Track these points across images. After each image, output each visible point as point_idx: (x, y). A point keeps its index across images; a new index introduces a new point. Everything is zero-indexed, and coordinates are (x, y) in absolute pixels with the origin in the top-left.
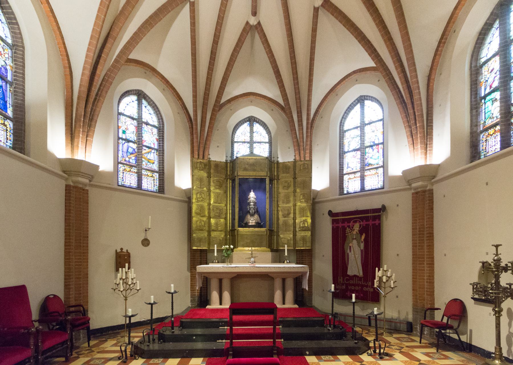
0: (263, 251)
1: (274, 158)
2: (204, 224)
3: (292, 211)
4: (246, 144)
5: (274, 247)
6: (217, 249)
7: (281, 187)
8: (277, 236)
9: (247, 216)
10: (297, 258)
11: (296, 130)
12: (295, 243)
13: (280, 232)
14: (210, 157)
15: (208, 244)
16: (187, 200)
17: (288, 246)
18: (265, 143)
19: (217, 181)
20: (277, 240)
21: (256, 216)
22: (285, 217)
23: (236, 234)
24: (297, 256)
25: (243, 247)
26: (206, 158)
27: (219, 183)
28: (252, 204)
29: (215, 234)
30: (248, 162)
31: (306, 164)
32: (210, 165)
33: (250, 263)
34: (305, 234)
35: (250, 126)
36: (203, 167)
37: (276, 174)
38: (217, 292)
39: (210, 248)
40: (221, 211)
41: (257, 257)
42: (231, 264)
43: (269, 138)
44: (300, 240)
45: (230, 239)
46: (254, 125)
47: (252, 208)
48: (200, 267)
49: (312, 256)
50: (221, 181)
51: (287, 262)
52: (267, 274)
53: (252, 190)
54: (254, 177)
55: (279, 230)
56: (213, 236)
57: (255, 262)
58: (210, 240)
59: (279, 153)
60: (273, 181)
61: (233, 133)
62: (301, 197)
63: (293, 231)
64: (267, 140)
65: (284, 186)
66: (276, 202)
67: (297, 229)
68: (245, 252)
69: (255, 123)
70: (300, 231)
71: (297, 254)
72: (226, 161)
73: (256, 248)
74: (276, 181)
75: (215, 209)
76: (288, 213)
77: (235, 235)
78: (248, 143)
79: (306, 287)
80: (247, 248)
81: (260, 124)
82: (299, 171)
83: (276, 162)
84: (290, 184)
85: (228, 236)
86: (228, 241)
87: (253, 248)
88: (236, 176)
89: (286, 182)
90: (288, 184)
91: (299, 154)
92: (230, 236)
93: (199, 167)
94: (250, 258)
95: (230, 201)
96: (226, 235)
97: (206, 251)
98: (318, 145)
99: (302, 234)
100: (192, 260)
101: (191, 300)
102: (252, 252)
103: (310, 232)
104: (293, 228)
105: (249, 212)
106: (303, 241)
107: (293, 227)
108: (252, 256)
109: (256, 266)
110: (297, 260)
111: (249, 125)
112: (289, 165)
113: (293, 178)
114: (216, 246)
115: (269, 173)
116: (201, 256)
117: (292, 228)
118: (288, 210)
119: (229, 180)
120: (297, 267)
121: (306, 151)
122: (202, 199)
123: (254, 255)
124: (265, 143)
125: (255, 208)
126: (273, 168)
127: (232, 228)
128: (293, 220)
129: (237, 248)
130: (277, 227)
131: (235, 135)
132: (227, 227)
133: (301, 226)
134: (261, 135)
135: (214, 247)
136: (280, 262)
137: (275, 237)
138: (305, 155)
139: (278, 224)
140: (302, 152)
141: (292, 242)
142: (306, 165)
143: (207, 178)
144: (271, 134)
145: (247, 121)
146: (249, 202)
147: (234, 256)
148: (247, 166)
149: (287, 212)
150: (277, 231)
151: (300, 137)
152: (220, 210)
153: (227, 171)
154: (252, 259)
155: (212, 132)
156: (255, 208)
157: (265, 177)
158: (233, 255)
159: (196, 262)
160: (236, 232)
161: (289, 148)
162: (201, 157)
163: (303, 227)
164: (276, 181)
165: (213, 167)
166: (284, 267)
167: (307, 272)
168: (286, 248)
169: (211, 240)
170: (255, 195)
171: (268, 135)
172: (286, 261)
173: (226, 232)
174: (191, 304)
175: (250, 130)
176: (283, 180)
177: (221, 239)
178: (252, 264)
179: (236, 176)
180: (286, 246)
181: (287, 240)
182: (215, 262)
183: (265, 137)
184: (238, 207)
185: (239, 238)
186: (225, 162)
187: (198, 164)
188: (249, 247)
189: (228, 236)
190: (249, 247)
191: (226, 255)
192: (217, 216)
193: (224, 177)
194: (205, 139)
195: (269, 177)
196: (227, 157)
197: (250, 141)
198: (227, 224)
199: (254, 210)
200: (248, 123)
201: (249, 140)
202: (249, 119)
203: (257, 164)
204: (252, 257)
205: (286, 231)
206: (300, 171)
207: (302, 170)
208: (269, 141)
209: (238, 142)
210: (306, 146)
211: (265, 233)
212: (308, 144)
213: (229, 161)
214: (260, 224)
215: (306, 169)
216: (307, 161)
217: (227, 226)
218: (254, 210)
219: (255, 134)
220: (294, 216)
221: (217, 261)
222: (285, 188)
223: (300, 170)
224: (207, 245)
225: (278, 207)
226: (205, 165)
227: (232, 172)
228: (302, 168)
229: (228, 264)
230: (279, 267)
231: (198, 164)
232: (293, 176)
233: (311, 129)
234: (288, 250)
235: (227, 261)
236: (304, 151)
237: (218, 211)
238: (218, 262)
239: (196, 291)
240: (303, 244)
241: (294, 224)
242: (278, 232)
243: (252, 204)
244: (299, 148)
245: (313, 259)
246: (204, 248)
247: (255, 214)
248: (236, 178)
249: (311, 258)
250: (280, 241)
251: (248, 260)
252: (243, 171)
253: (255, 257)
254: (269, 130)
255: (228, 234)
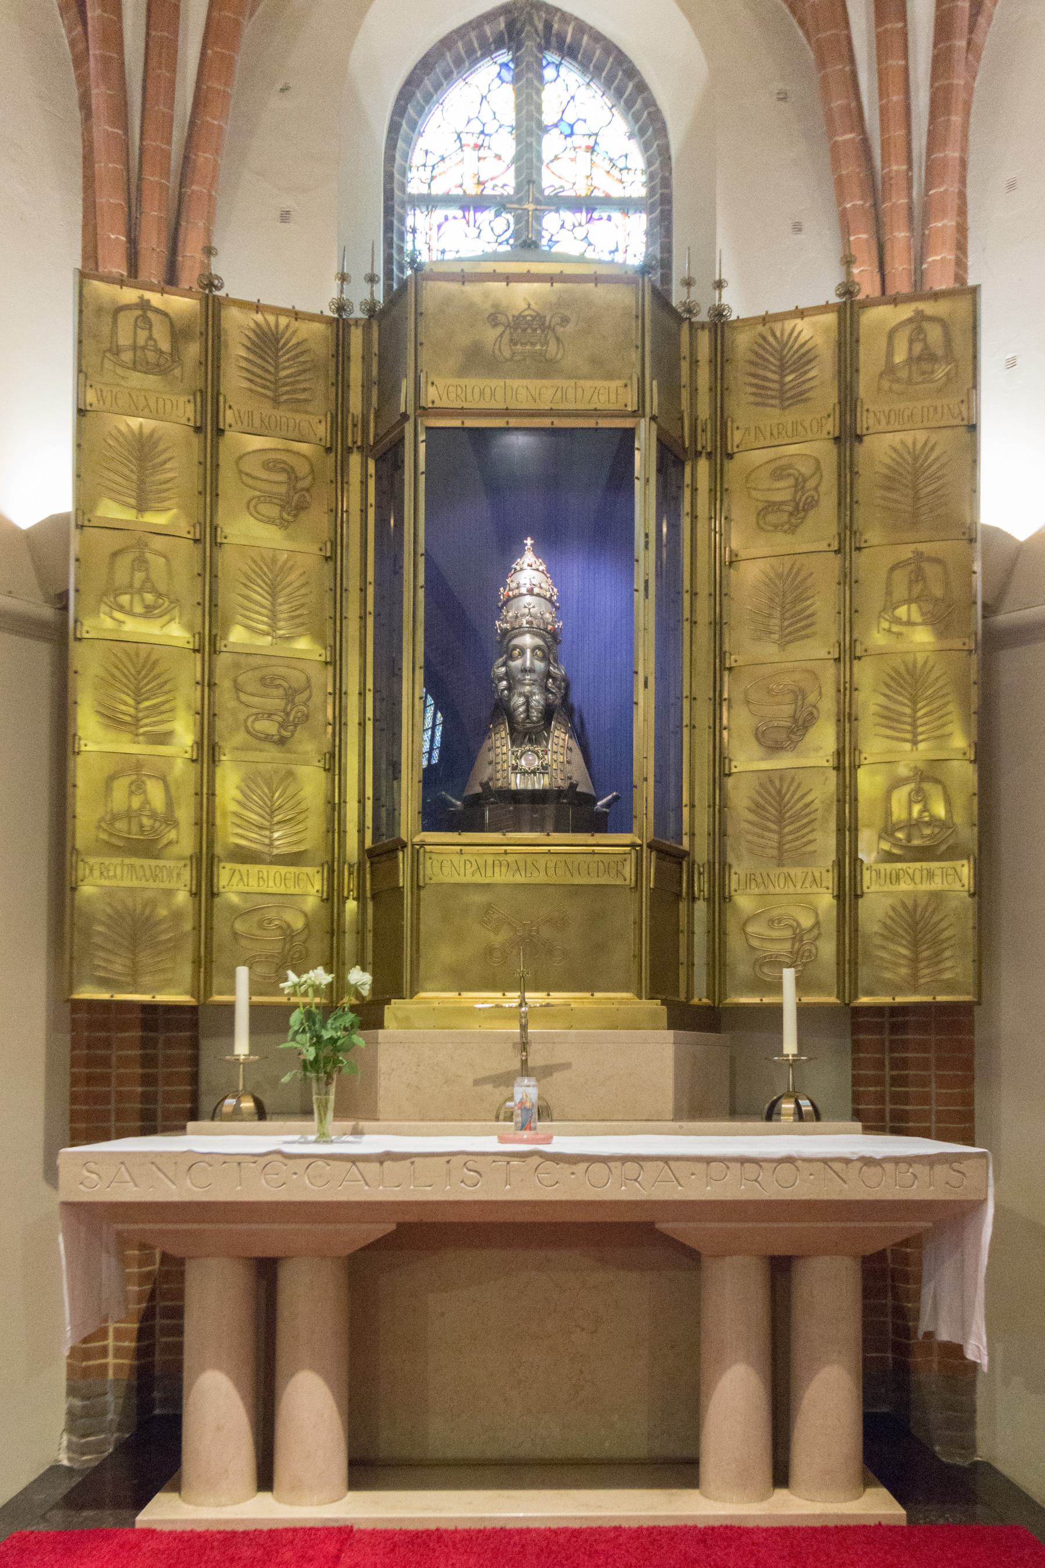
0: (613, 1022)
1: (688, 283)
2: (170, 804)
3: (828, 706)
4: (489, 214)
5: (690, 994)
6: (253, 1008)
7: (740, 509)
8: (710, 900)
9: (488, 743)
10: (856, 1081)
11: (852, 60)
12: (854, 963)
13: (739, 869)
14: (218, 267)
15: (197, 962)
16: (48, 613)
17: (802, 984)
18: (625, 206)
19: (266, 466)
20: (710, 932)
21: (560, 737)
22: (774, 748)
23: (404, 880)
24: (856, 1064)
25: (460, 990)
26: (189, 277)
27: (282, 477)
28: (527, 640)
29: (254, 886)
30: (496, 306)
31: (932, 319)
32: (218, 336)
33: (510, 1117)
34: (926, 887)
35: (516, 79)
36: (165, 346)
37: (704, 411)
38: (237, 1384)
39: (208, 992)
40: (298, 699)
41: (565, 1066)
42: (357, 1132)
43: (649, 163)
44: (889, 934)
45: (364, 922)
46: (549, 73)
47: (524, 671)
48: (86, 1161)
49: (968, 1065)
50: (303, 469)
51: (800, 1115)
52: (644, 1217)
53: (529, 542)
54: (545, 422)
55: (731, 858)
56: (235, 899)
57: (544, 1112)
58: (210, 929)
59: (722, 242)
60: (688, 470)
61: (394, 129)
62: (900, 591)
63: (839, 864)
64: (637, 187)
65: (770, 507)
66: (704, 634)
67: (867, 854)
68: (475, 1028)
69: (551, 57)
70: (889, 857)
71: (857, 1047)
72: (341, 307)
73: (558, 997)
74: (703, 466)
75: (249, 689)
76: (794, 718)
77: (399, 890)
78: (501, 205)
79: (963, 1324)
80: (484, 1000)
81: (584, 67)
82: (881, 375)
83: (703, 317)
84: (811, 484)
85: (351, 905)
86: (349, 942)
87: (535, 998)
88: (405, 417)
89: (779, 473)
90: (800, 484)
91: (874, 253)
92: (360, 898)
93: (134, 347)
94: (506, 1080)
95: (364, 627)
96: (332, 898)
97: (194, 1025)
98: (1011, 186)
99: (905, 886)
100: (81, 1089)
101: (71, 1414)
102: (524, 1028)
103: (965, 870)
104: (832, 841)
105: (502, 710)
106: (915, 945)
107: (833, 826)
108: (524, 1062)
109: (563, 1144)
110: (856, 1098)
111: (507, 76)
112: (805, 336)
113: (837, 439)
114: (242, 974)
115: (653, 387)
116: (148, 1061)
117: (826, 842)
118: (799, 694)
119: (355, 460)
120: (896, 1160)
121: (926, 222)
122: (149, 598)
123: (535, 1060)
124: (625, 206)
125: (548, 675)
126: (685, 365)
127: (374, 840)
128: (833, 775)
129: (412, 995)
130: (711, 834)
131: (409, 142)
132: (342, 832)
133: (898, 812)
134: (591, 149)
135: (232, 991)
136: (735, 1112)
137: (701, 908)
138: (920, 258)
139: (720, 808)
140: (900, 236)
141: (827, 949)
142: (934, 334)
143: (195, 440)
144: (662, 131)
145: (500, 43)
146: (505, 632)
147: (383, 1064)
148: (490, 335)
149: (787, 710)
150: (711, 864)
151: (883, 111)
152: (290, 695)
153: (346, 386)
154: (526, 1091)
155: (228, 63)
156: (548, 675)
157: (627, 423)
158: (381, 1048)
159: (112, 1106)
160: (404, 860)
161: (797, 228)
162: (152, 267)
163: (912, 826)
164: (703, 466)
165: (236, 350)
166: (789, 1160)
167: (976, 1206)
168: (789, 999)
169: (222, 931)
170: (551, 572)
171: (646, 147)
172: (788, 1106)
173: (332, 870)
174: (70, 1447)
175: (518, 108)
176: (758, 457)
177: (298, 924)
178: (523, 1127)
179: (405, 417)
180: (789, 976)
181: (788, 933)
182: (236, 1114)
183: (621, 163)
184: (420, 661)
185: (430, 920)
186: (329, 321)
187: (126, 322)
188: (504, 988)
189: (351, 905)
190: (504, 987)
191: (310, 1054)
192: (267, 738)
193: (322, 430)
194: (178, 135)
195: (653, 418)
196: (343, 278)
197: (518, 188)
198: (343, 802)
199: (547, 690)
200: (504, 56)
201: (512, 183)
202: (510, 25)
203: (565, 320)
204: (525, 1070)
205: (780, 864)
206: (886, 384)
207: (903, 374)
208: (652, 192)
209: (429, 202)
210: (929, 185)
211: (629, 871)
212: (944, 160)
213: (358, 314)
214: (589, 800)
215: (932, 358)
216: (936, 296)
217: (342, 821)
218: (547, 690)
219: (551, 144)
220: (840, 736)
221: (248, 1104)
222: (771, 518)
223: (890, 369)
224: (186, 971)
225: (723, 668)
226: (178, 333)
227: (381, 394)
228: (899, 358)
229: (332, 1125)
230: (743, 1160)
231: (126, 322)
232: (831, 426)
233: (972, 28)
234: (802, 1011)
235: (324, 1106)
236: (911, 228)
237: (275, 702)
238: (261, 1113)
239: (110, 1342)
240: (914, 961)
241: (840, 801)
242: (719, 869)
243: (527, 640)
244: (875, 205)
245: (977, 1089)
246: (162, 998)
247: (547, 726)
248: (409, 427)
249: (968, 1081)
250: (735, 942)
251: (497, 1094)
252: (463, 371)
253: (546, 1072)
254: (650, 103)
255: (350, 883)
